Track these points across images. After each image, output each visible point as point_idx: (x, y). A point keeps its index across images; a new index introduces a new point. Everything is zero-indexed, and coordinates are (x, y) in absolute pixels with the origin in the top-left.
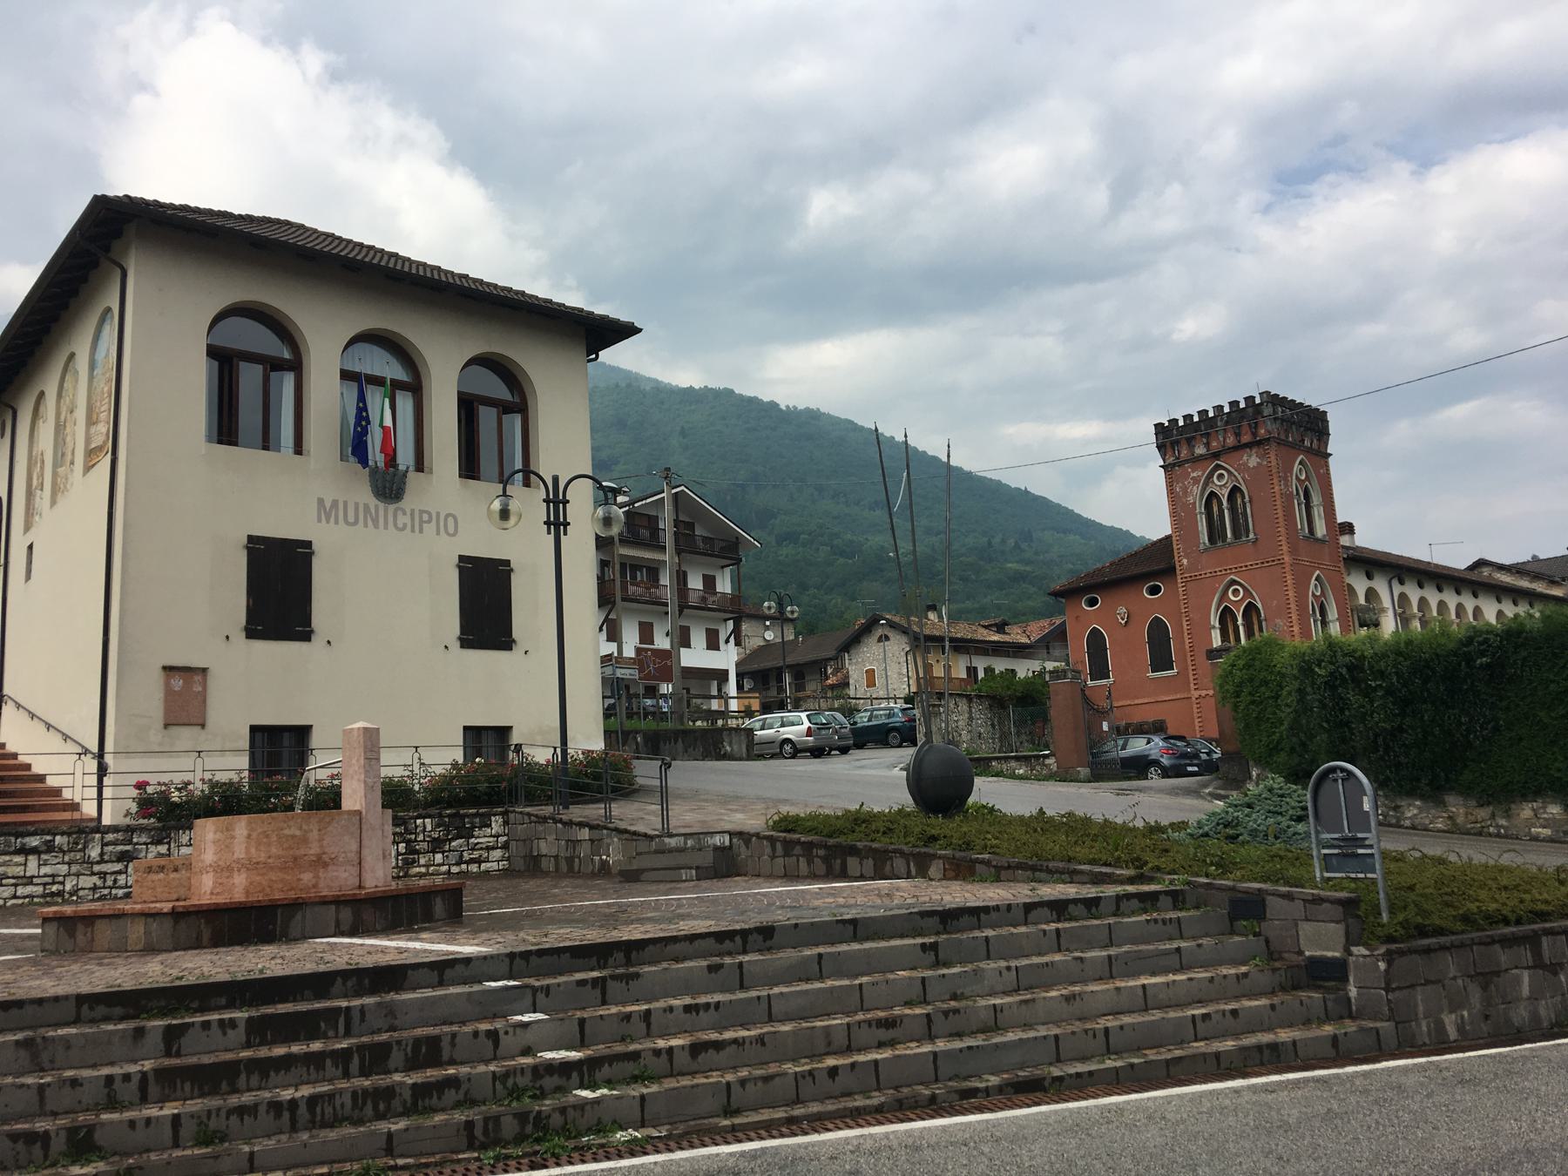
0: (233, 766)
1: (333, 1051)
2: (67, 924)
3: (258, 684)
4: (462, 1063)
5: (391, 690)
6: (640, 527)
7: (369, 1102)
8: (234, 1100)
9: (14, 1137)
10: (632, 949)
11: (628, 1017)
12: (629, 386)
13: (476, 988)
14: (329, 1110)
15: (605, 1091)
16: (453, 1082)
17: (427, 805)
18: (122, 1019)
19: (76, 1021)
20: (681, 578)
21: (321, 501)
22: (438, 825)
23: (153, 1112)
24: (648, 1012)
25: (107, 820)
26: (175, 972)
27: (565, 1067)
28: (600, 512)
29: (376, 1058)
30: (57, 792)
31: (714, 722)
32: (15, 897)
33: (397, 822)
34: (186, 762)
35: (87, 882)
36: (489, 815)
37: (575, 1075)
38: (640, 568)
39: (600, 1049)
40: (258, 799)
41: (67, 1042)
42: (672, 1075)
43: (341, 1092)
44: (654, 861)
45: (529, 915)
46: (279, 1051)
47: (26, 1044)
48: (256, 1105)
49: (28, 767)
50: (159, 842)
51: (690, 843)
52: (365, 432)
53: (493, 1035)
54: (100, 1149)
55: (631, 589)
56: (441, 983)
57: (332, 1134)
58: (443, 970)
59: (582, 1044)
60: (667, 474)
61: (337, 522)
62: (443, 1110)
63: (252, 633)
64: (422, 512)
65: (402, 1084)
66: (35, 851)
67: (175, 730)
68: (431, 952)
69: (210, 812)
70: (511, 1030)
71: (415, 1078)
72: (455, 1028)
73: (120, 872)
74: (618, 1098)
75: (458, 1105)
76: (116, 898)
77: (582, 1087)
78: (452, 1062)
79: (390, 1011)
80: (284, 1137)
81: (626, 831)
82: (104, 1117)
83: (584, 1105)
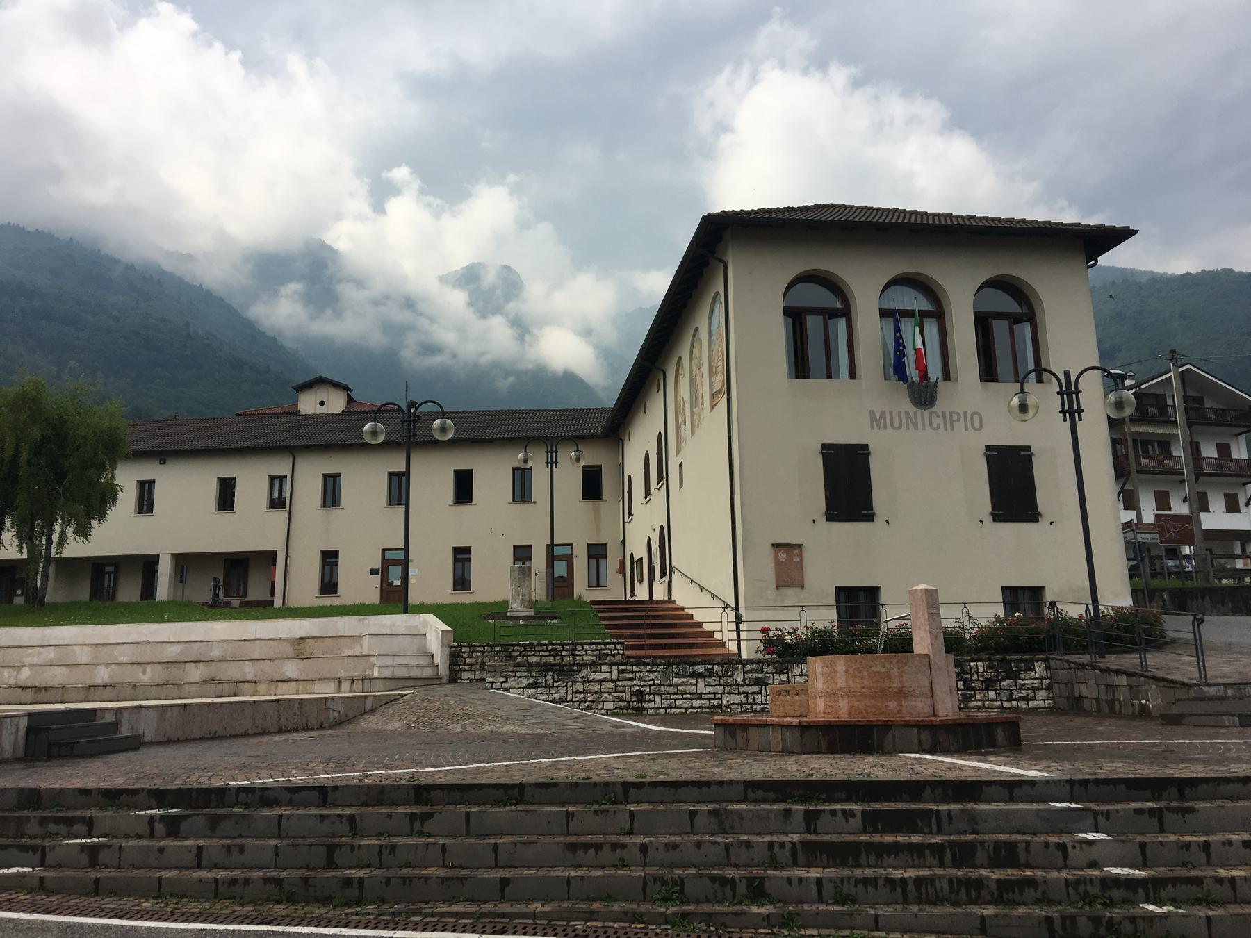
0: (826, 617)
1: (930, 845)
2: (730, 729)
3: (839, 555)
4: (1037, 868)
5: (941, 561)
6: (1151, 406)
7: (963, 891)
8: (858, 872)
9: (713, 879)
10: (1183, 785)
11: (1187, 846)
12: (1125, 281)
13: (1042, 806)
14: (931, 891)
15: (1171, 908)
16: (1031, 882)
17: (978, 651)
18: (775, 801)
19: (745, 800)
20: (1195, 449)
21: (872, 413)
22: (989, 668)
23: (802, 873)
24: (1207, 844)
25: (744, 656)
26: (807, 770)
27: (1130, 882)
28: (1112, 397)
29: (964, 855)
30: (711, 634)
31: (1241, 580)
32: (692, 707)
33: (958, 664)
34: (794, 614)
35: (737, 699)
36: (1032, 661)
37: (1140, 890)
38: (1151, 442)
39: (1162, 871)
40: (847, 643)
41: (740, 814)
42: (1235, 902)
43: (940, 877)
44: (1189, 708)
45: (1080, 748)
46: (889, 839)
47: (714, 813)
48: (876, 879)
49: (691, 616)
50: (781, 672)
51: (1230, 692)
52: (903, 354)
53: (1062, 847)
54: (769, 896)
55: (1144, 462)
56: (1011, 799)
57: (937, 910)
58: (1012, 788)
59: (1144, 865)
60: (1173, 357)
61: (885, 428)
62: (1025, 904)
63: (830, 517)
64: (951, 413)
65: (988, 878)
66: (701, 675)
67: (784, 590)
68: (1001, 772)
69: (815, 652)
70: (1077, 845)
71: (997, 875)
72: (1028, 838)
73: (756, 693)
74: (1183, 916)
75: (1037, 902)
76: (756, 711)
77: (1149, 902)
78: (1029, 866)
79: (972, 818)
80: (899, 907)
81: (1163, 679)
82: (770, 872)
83: (1152, 917)
